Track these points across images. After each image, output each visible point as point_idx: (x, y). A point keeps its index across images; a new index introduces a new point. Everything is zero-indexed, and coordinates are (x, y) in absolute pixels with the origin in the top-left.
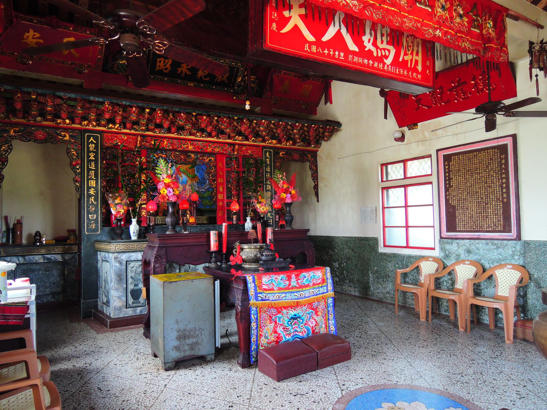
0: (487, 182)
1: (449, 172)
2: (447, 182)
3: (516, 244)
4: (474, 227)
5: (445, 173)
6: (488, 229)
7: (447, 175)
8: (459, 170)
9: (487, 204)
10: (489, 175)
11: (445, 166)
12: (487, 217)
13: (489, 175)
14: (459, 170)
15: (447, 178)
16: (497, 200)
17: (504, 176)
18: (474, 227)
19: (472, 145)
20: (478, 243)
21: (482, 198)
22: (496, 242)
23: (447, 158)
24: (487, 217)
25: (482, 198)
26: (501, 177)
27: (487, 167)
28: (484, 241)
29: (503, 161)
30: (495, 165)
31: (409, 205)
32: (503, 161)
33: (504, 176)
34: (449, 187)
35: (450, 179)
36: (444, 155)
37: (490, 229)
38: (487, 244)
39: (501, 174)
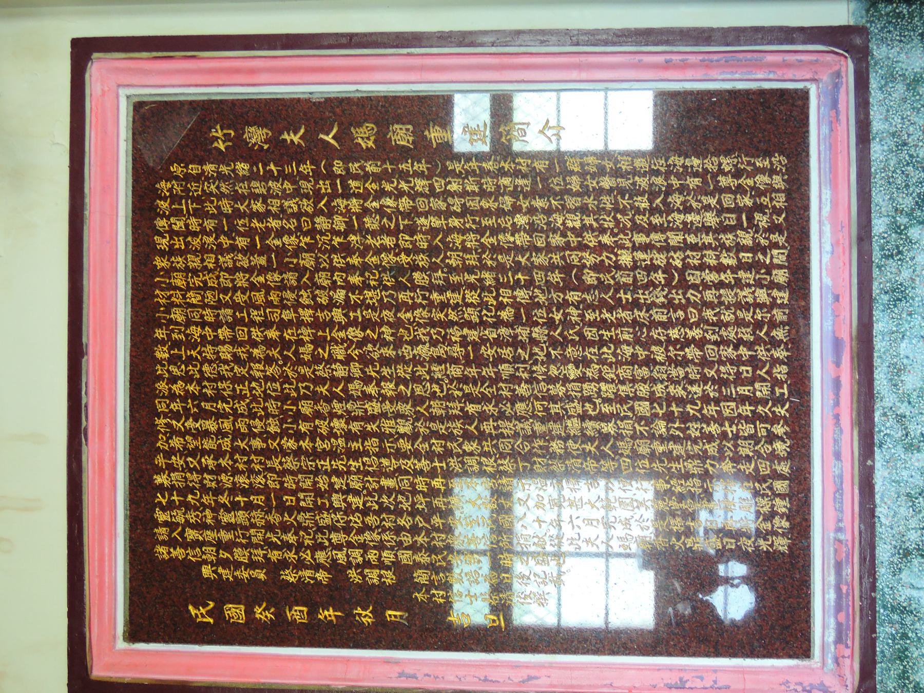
0: (398, 270)
1: (277, 593)
2: (366, 616)
3: (891, 77)
4: (762, 390)
5: (280, 633)
6: (781, 276)
7: (297, 613)
8: (276, 501)
9: (572, 277)
10: (347, 250)
11: (223, 633)
12: (677, 279)
13: (347, 250)
14: (276, 501)
15: (329, 614)
16: (547, 192)
17: (364, 136)
18: (762, 390)
19: (90, 364)
20: (897, 370)
21: (524, 314)
22: (879, 225)
23: (172, 138)
24: (677, 279)
25: (524, 314)
26: (369, 155)
27: (281, 260)
28: (881, 324)
29: (256, 135)
30: (276, 198)
31: (610, 560)
32: (256, 135)
33: (364, 136)
34: (407, 604)
35: (340, 590)
36: (134, 634)
37: (779, 257)
38: (899, 294)
39: (351, 153)
